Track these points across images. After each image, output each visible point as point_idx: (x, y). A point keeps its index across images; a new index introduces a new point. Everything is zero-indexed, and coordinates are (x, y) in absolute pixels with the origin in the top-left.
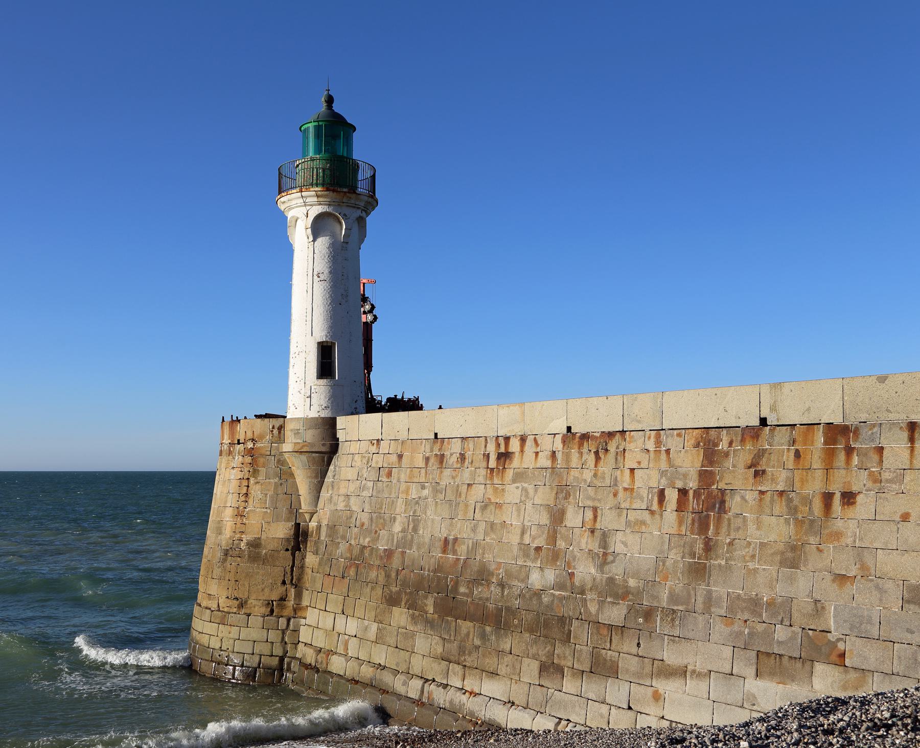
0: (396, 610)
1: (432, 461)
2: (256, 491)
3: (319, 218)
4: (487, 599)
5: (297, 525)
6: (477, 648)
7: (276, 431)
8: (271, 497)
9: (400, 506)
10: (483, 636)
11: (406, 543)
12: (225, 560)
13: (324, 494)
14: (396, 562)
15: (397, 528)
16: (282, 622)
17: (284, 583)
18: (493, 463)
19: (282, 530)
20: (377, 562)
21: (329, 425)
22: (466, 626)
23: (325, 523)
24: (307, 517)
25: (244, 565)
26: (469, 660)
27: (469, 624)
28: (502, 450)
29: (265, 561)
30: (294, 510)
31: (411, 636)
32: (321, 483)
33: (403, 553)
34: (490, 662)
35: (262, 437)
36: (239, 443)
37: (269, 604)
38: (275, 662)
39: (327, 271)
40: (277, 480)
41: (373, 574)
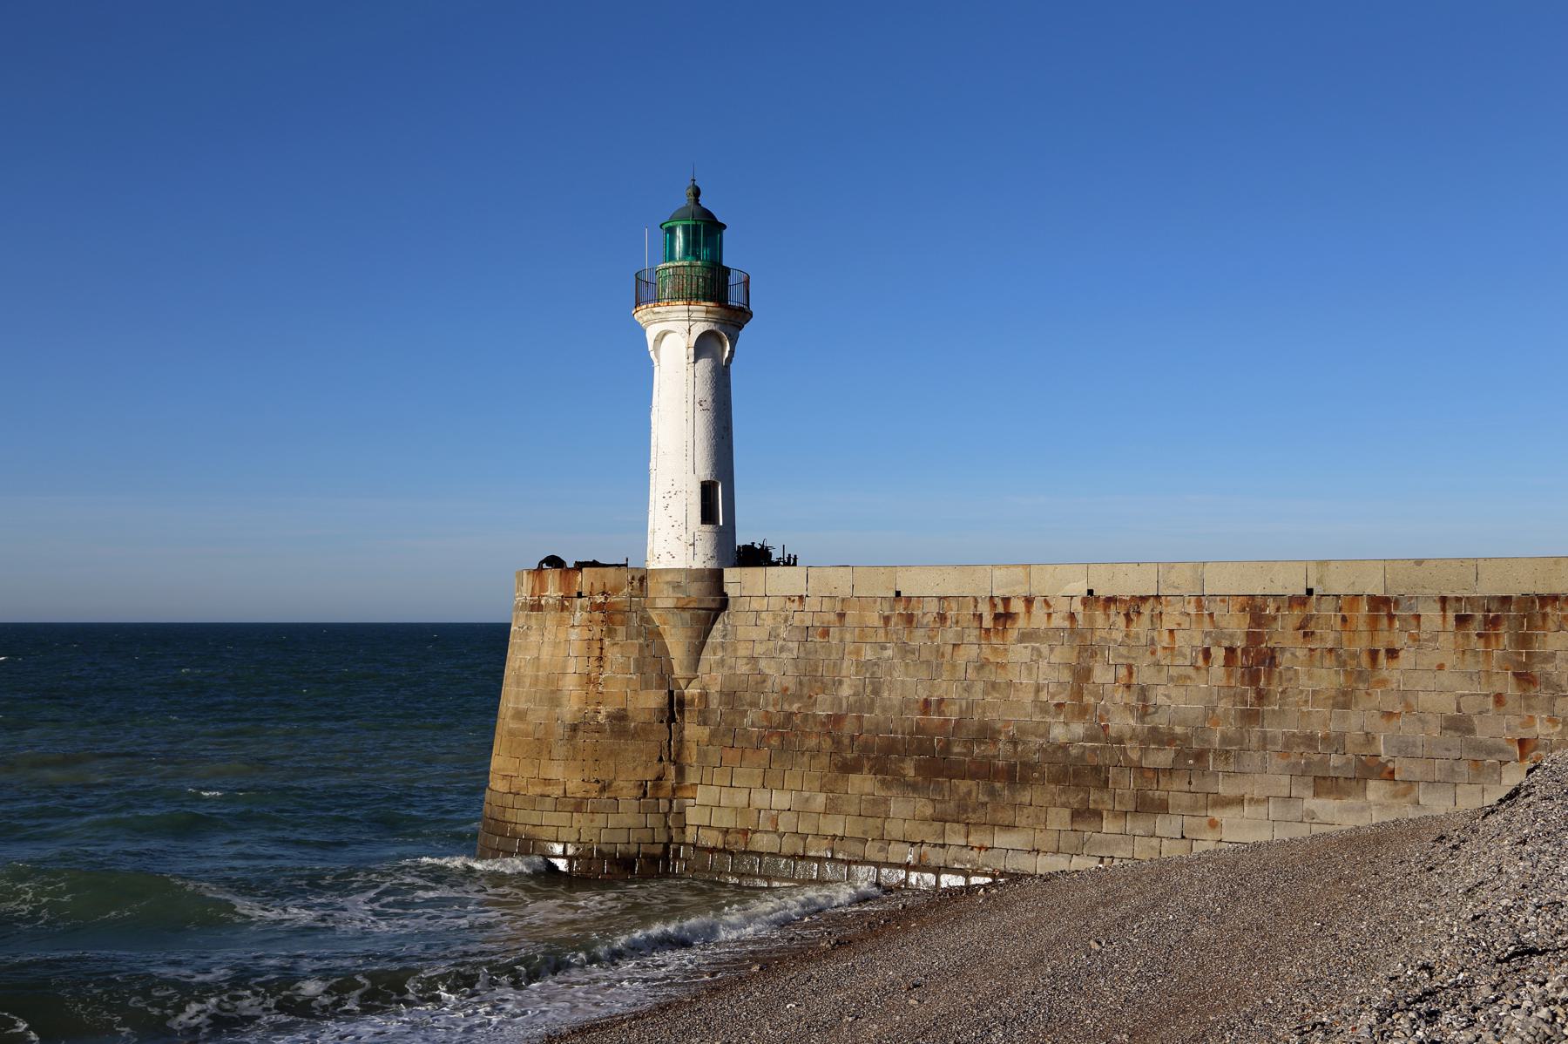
0: (854, 778)
1: (893, 621)
2: (613, 654)
3: (703, 337)
4: (994, 757)
5: (671, 693)
6: (984, 804)
7: (636, 583)
8: (636, 660)
9: (848, 667)
10: (992, 793)
11: (860, 706)
12: (572, 738)
13: (708, 657)
14: (849, 727)
15: (846, 691)
16: (663, 804)
17: (661, 760)
18: (988, 622)
19: (654, 699)
20: (817, 729)
21: (716, 577)
22: (963, 785)
23: (714, 690)
24: (682, 683)
25: (606, 741)
26: (973, 818)
27: (969, 782)
28: (1000, 609)
29: (635, 735)
30: (665, 677)
31: (886, 801)
32: (703, 644)
33: (859, 718)
34: (1006, 816)
35: (616, 590)
36: (580, 595)
37: (642, 785)
38: (658, 849)
39: (710, 399)
40: (641, 640)
41: (812, 742)
